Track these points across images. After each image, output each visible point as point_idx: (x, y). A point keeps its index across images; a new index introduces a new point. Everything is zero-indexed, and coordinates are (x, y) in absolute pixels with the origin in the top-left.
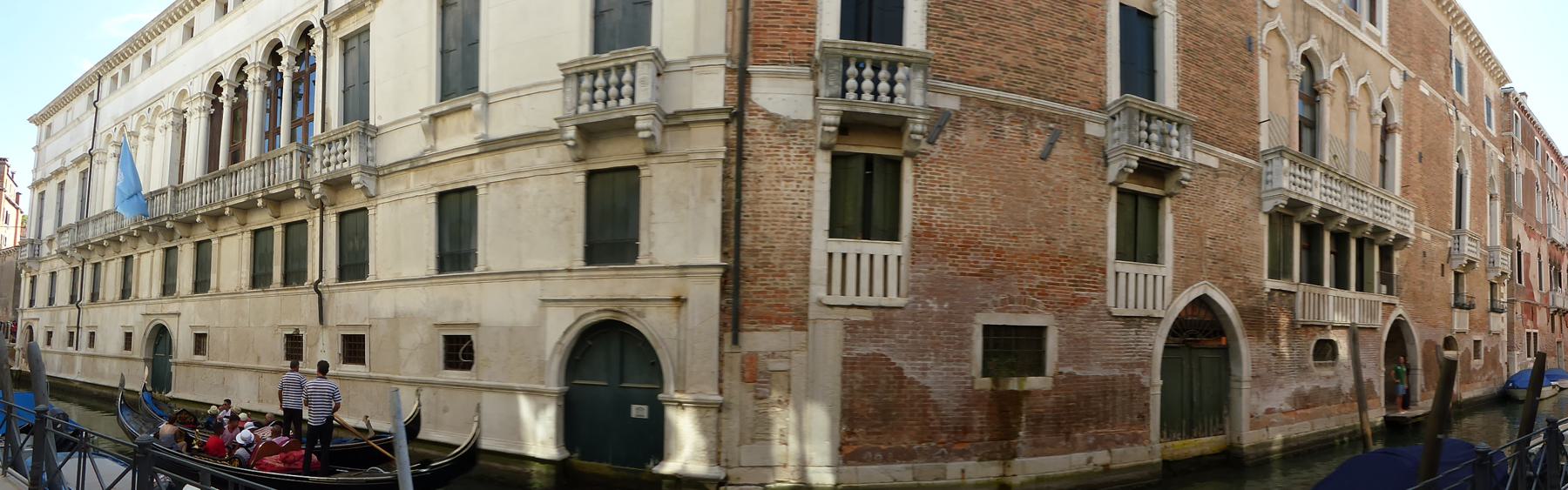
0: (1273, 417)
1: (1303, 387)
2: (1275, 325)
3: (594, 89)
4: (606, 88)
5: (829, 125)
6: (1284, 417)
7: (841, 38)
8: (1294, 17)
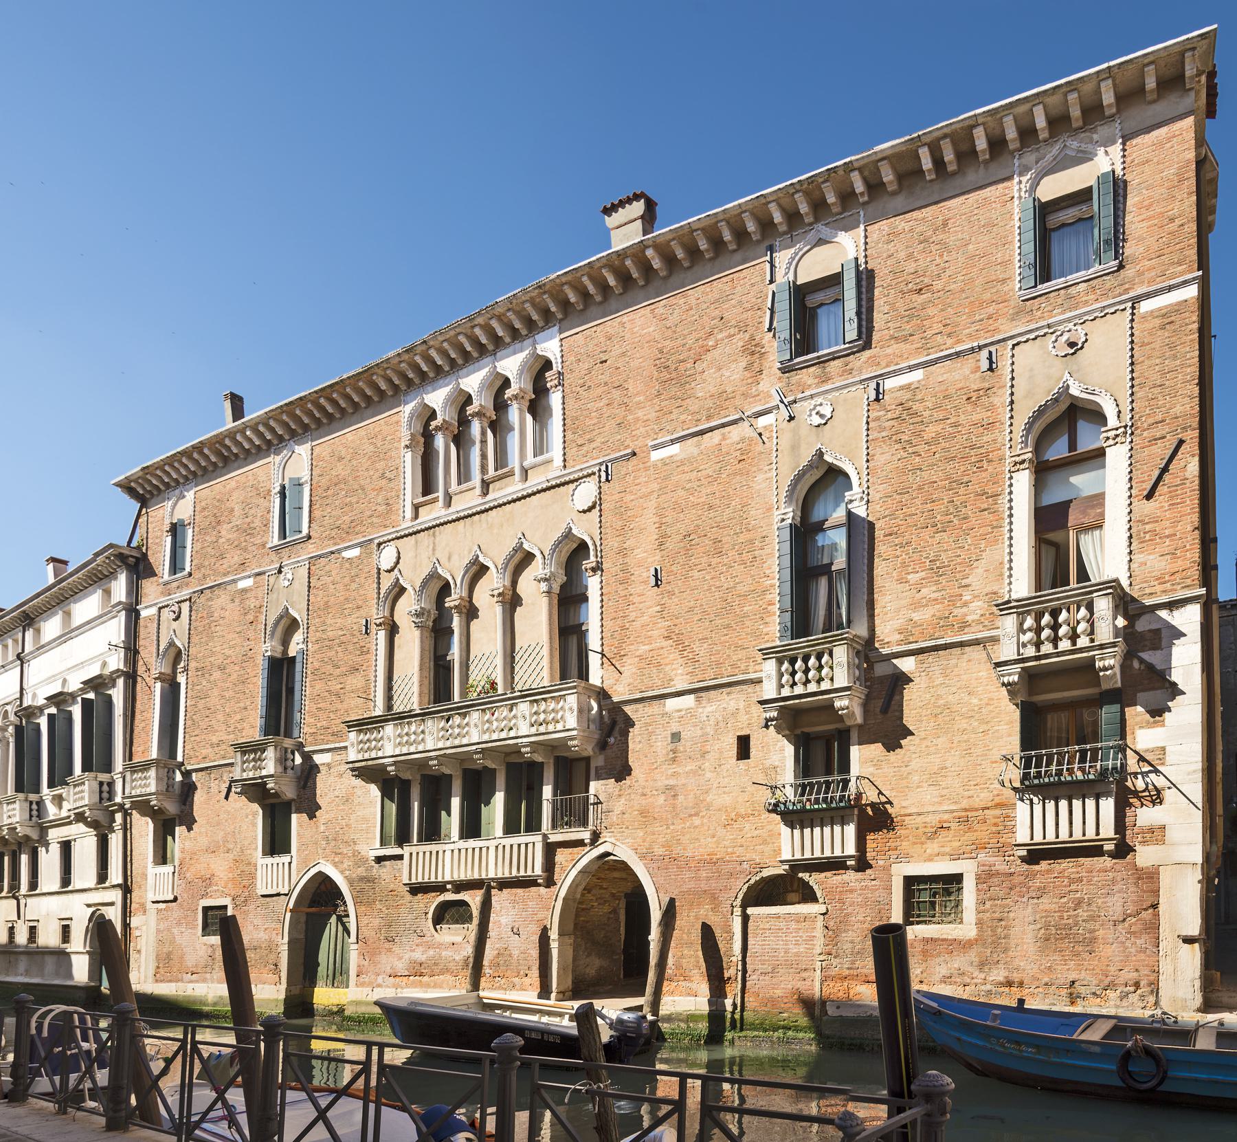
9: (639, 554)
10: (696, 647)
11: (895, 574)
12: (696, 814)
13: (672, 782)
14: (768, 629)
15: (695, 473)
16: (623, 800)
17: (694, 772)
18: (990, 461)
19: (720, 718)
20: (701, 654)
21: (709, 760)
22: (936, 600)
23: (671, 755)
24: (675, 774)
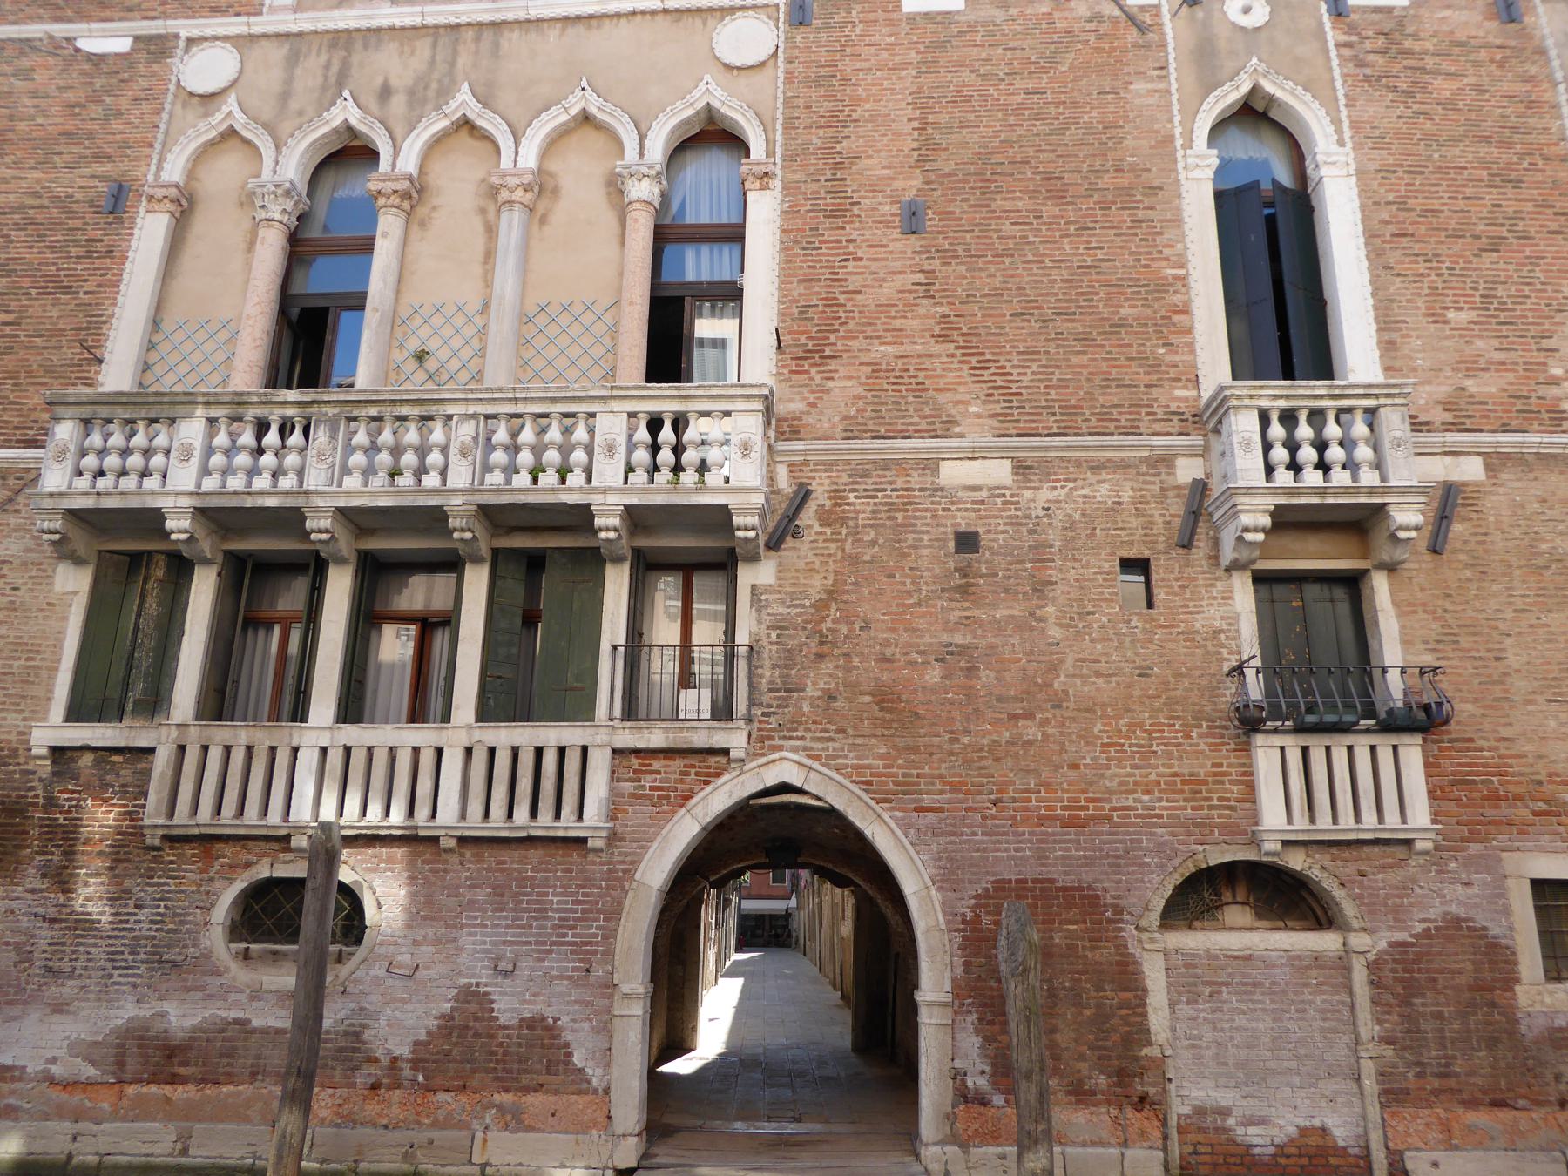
0: (12, 1092)
1: (163, 1014)
2: (65, 837)
3: (260, 451)
4: (397, 451)
5: (1256, 530)
6: (56, 1095)
7: (1234, 378)
8: (289, 81)
9: (873, 166)
10: (1011, 363)
11: (1420, 303)
12: (1029, 716)
13: (959, 639)
14: (1177, 358)
15: (1000, 51)
16: (827, 667)
17: (1021, 626)
18: (1546, 158)
19: (1077, 516)
20: (1026, 381)
21: (1054, 599)
22: (1503, 363)
23: (957, 580)
24: (968, 623)
